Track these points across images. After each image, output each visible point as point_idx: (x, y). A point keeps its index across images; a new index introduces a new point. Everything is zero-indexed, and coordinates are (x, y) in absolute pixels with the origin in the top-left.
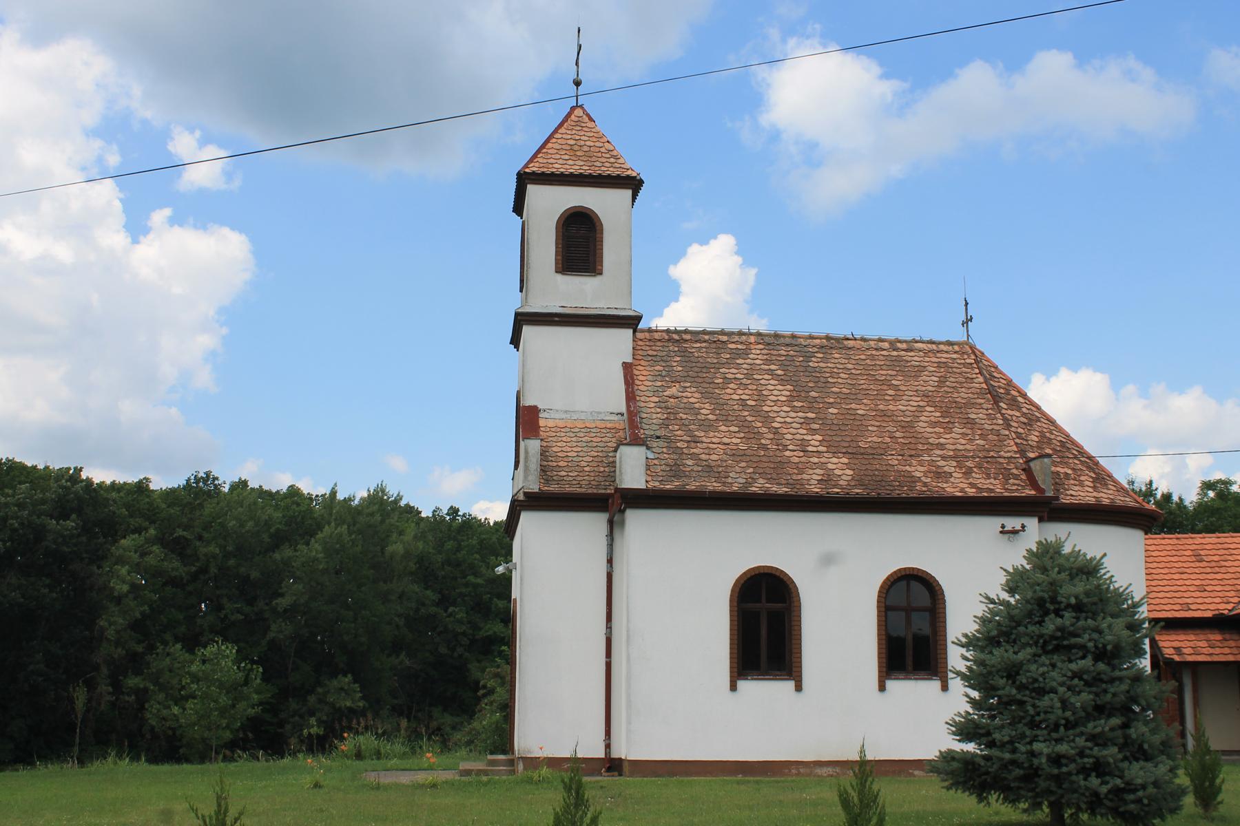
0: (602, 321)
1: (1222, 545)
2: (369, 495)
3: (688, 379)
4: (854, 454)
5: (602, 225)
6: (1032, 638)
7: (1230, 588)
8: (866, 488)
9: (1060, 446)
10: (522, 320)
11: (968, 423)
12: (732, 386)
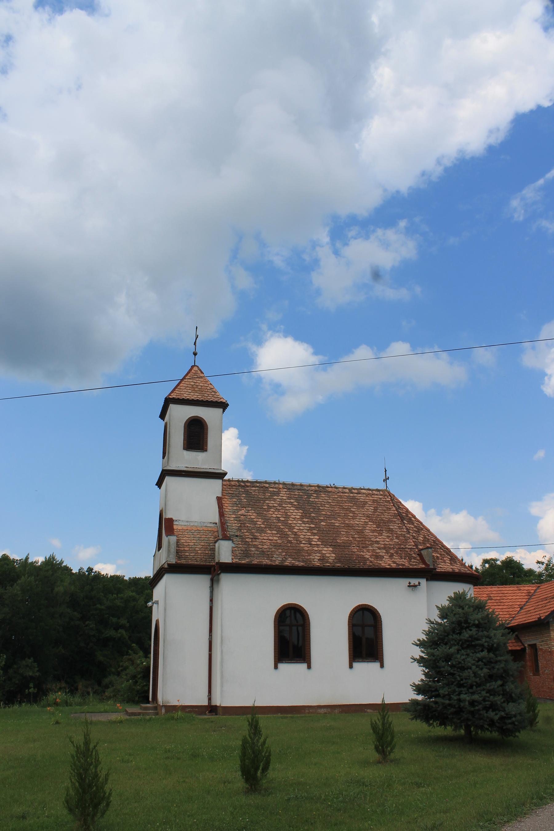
1: (501, 592)
2: (46, 560)
3: (250, 506)
4: (336, 546)
5: (207, 426)
6: (456, 641)
7: (506, 613)
8: (342, 564)
9: (433, 543)
10: (165, 473)
11: (389, 530)
12: (272, 510)
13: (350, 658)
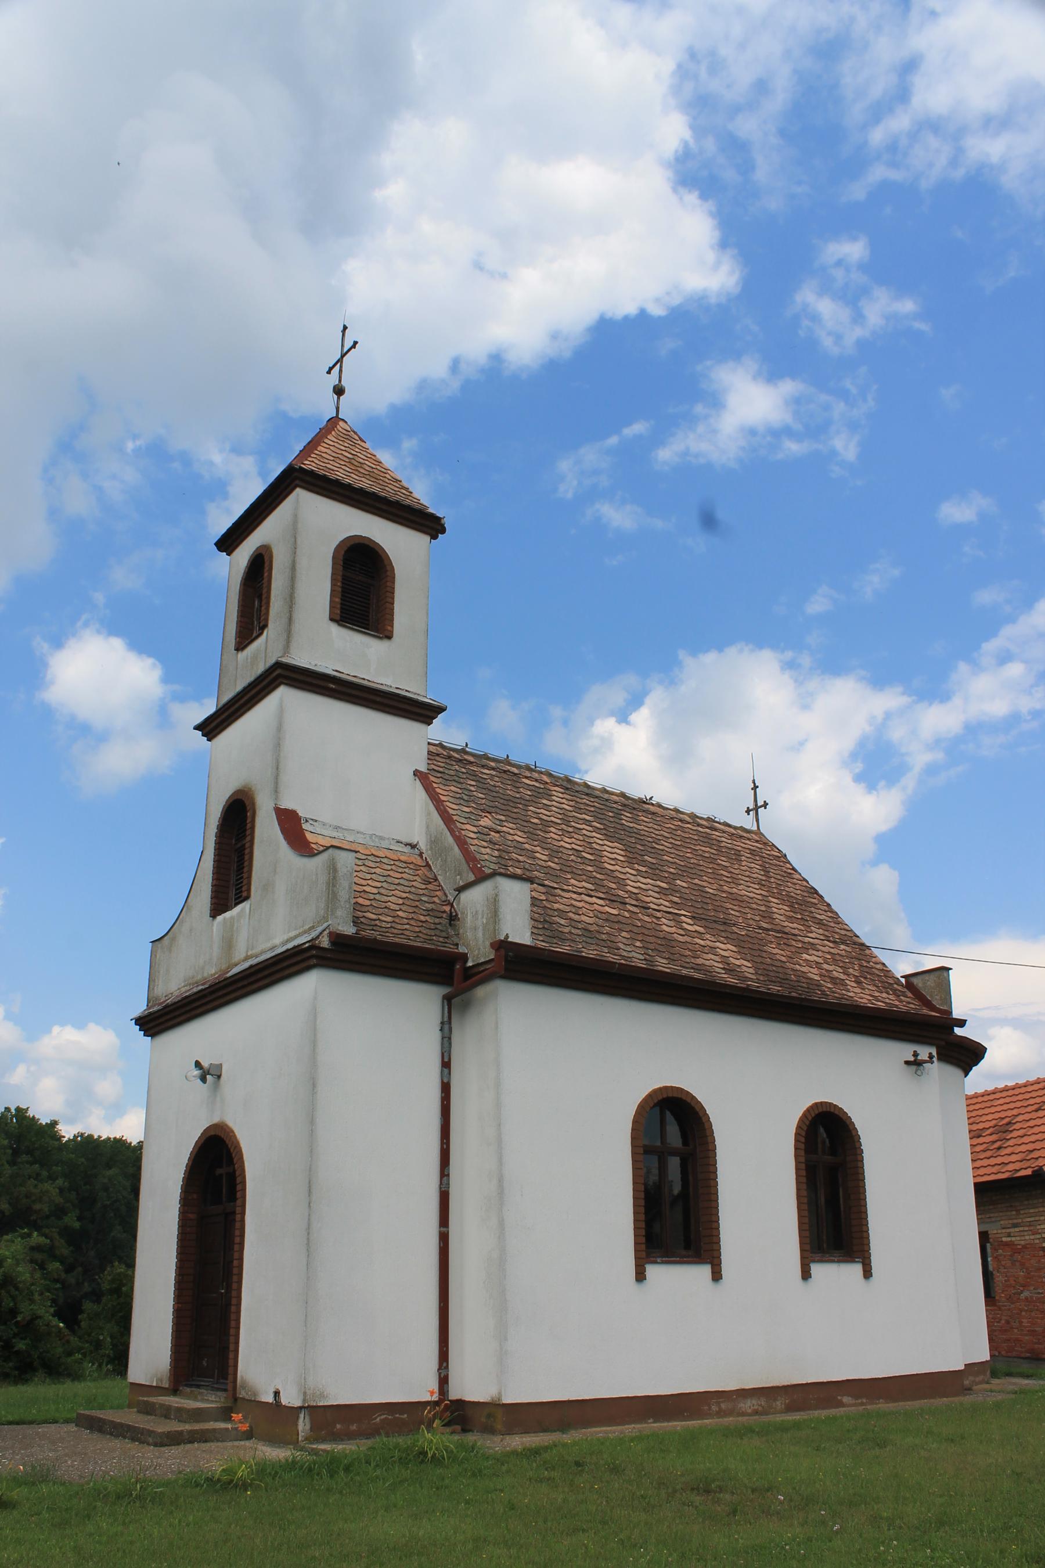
13: (802, 1250)
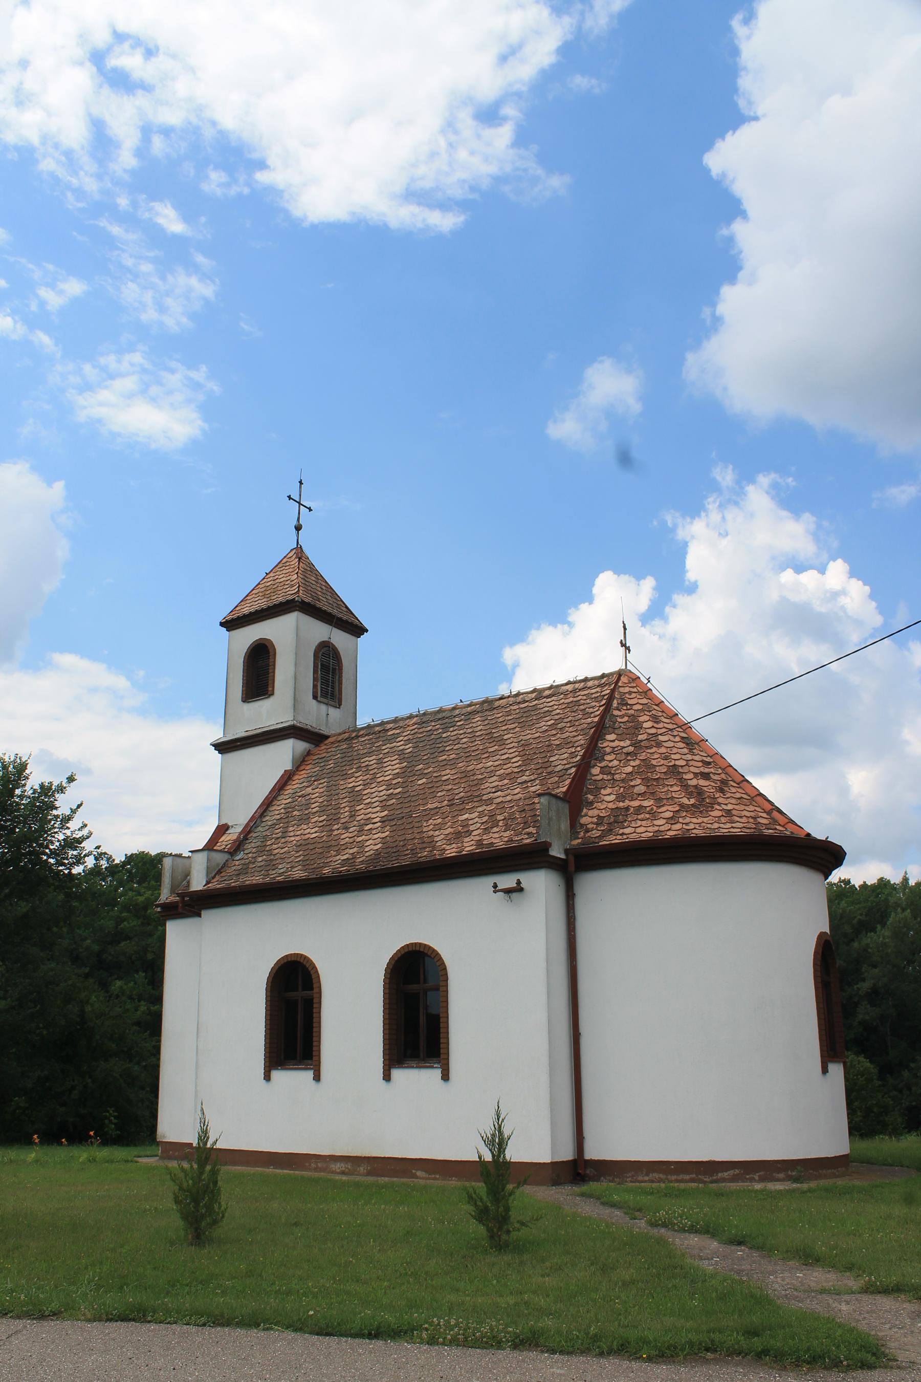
0: (257, 739)
